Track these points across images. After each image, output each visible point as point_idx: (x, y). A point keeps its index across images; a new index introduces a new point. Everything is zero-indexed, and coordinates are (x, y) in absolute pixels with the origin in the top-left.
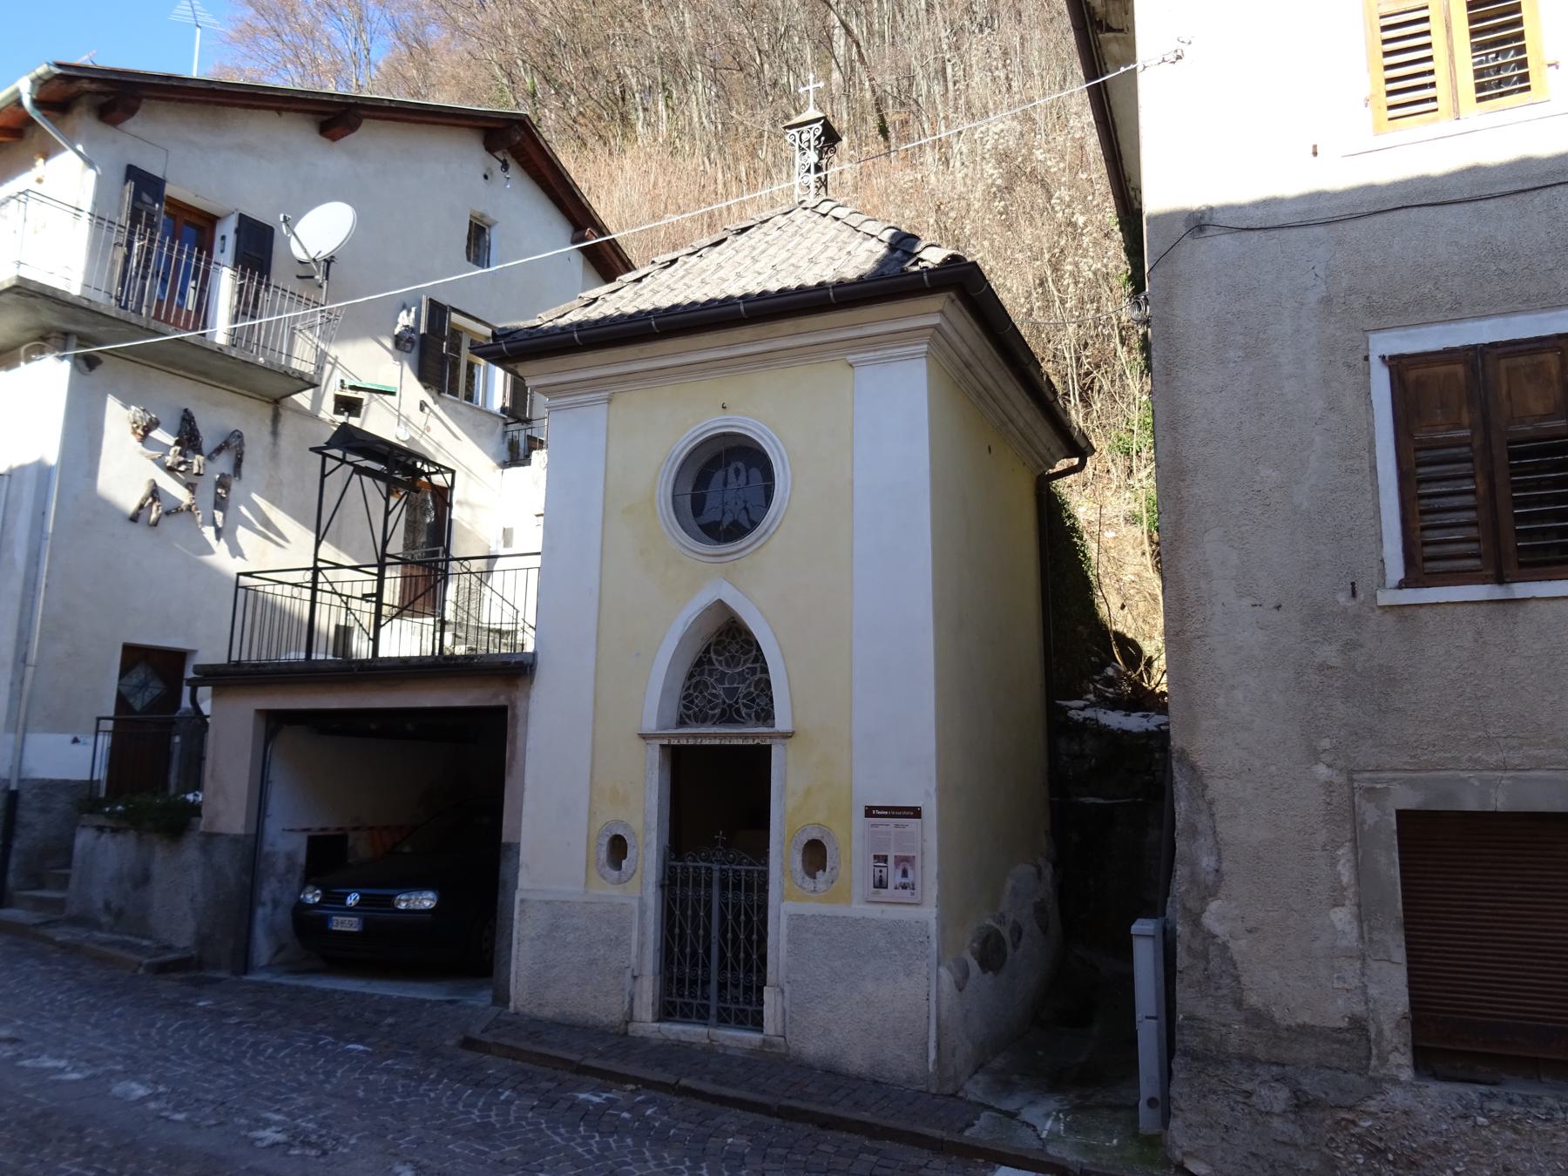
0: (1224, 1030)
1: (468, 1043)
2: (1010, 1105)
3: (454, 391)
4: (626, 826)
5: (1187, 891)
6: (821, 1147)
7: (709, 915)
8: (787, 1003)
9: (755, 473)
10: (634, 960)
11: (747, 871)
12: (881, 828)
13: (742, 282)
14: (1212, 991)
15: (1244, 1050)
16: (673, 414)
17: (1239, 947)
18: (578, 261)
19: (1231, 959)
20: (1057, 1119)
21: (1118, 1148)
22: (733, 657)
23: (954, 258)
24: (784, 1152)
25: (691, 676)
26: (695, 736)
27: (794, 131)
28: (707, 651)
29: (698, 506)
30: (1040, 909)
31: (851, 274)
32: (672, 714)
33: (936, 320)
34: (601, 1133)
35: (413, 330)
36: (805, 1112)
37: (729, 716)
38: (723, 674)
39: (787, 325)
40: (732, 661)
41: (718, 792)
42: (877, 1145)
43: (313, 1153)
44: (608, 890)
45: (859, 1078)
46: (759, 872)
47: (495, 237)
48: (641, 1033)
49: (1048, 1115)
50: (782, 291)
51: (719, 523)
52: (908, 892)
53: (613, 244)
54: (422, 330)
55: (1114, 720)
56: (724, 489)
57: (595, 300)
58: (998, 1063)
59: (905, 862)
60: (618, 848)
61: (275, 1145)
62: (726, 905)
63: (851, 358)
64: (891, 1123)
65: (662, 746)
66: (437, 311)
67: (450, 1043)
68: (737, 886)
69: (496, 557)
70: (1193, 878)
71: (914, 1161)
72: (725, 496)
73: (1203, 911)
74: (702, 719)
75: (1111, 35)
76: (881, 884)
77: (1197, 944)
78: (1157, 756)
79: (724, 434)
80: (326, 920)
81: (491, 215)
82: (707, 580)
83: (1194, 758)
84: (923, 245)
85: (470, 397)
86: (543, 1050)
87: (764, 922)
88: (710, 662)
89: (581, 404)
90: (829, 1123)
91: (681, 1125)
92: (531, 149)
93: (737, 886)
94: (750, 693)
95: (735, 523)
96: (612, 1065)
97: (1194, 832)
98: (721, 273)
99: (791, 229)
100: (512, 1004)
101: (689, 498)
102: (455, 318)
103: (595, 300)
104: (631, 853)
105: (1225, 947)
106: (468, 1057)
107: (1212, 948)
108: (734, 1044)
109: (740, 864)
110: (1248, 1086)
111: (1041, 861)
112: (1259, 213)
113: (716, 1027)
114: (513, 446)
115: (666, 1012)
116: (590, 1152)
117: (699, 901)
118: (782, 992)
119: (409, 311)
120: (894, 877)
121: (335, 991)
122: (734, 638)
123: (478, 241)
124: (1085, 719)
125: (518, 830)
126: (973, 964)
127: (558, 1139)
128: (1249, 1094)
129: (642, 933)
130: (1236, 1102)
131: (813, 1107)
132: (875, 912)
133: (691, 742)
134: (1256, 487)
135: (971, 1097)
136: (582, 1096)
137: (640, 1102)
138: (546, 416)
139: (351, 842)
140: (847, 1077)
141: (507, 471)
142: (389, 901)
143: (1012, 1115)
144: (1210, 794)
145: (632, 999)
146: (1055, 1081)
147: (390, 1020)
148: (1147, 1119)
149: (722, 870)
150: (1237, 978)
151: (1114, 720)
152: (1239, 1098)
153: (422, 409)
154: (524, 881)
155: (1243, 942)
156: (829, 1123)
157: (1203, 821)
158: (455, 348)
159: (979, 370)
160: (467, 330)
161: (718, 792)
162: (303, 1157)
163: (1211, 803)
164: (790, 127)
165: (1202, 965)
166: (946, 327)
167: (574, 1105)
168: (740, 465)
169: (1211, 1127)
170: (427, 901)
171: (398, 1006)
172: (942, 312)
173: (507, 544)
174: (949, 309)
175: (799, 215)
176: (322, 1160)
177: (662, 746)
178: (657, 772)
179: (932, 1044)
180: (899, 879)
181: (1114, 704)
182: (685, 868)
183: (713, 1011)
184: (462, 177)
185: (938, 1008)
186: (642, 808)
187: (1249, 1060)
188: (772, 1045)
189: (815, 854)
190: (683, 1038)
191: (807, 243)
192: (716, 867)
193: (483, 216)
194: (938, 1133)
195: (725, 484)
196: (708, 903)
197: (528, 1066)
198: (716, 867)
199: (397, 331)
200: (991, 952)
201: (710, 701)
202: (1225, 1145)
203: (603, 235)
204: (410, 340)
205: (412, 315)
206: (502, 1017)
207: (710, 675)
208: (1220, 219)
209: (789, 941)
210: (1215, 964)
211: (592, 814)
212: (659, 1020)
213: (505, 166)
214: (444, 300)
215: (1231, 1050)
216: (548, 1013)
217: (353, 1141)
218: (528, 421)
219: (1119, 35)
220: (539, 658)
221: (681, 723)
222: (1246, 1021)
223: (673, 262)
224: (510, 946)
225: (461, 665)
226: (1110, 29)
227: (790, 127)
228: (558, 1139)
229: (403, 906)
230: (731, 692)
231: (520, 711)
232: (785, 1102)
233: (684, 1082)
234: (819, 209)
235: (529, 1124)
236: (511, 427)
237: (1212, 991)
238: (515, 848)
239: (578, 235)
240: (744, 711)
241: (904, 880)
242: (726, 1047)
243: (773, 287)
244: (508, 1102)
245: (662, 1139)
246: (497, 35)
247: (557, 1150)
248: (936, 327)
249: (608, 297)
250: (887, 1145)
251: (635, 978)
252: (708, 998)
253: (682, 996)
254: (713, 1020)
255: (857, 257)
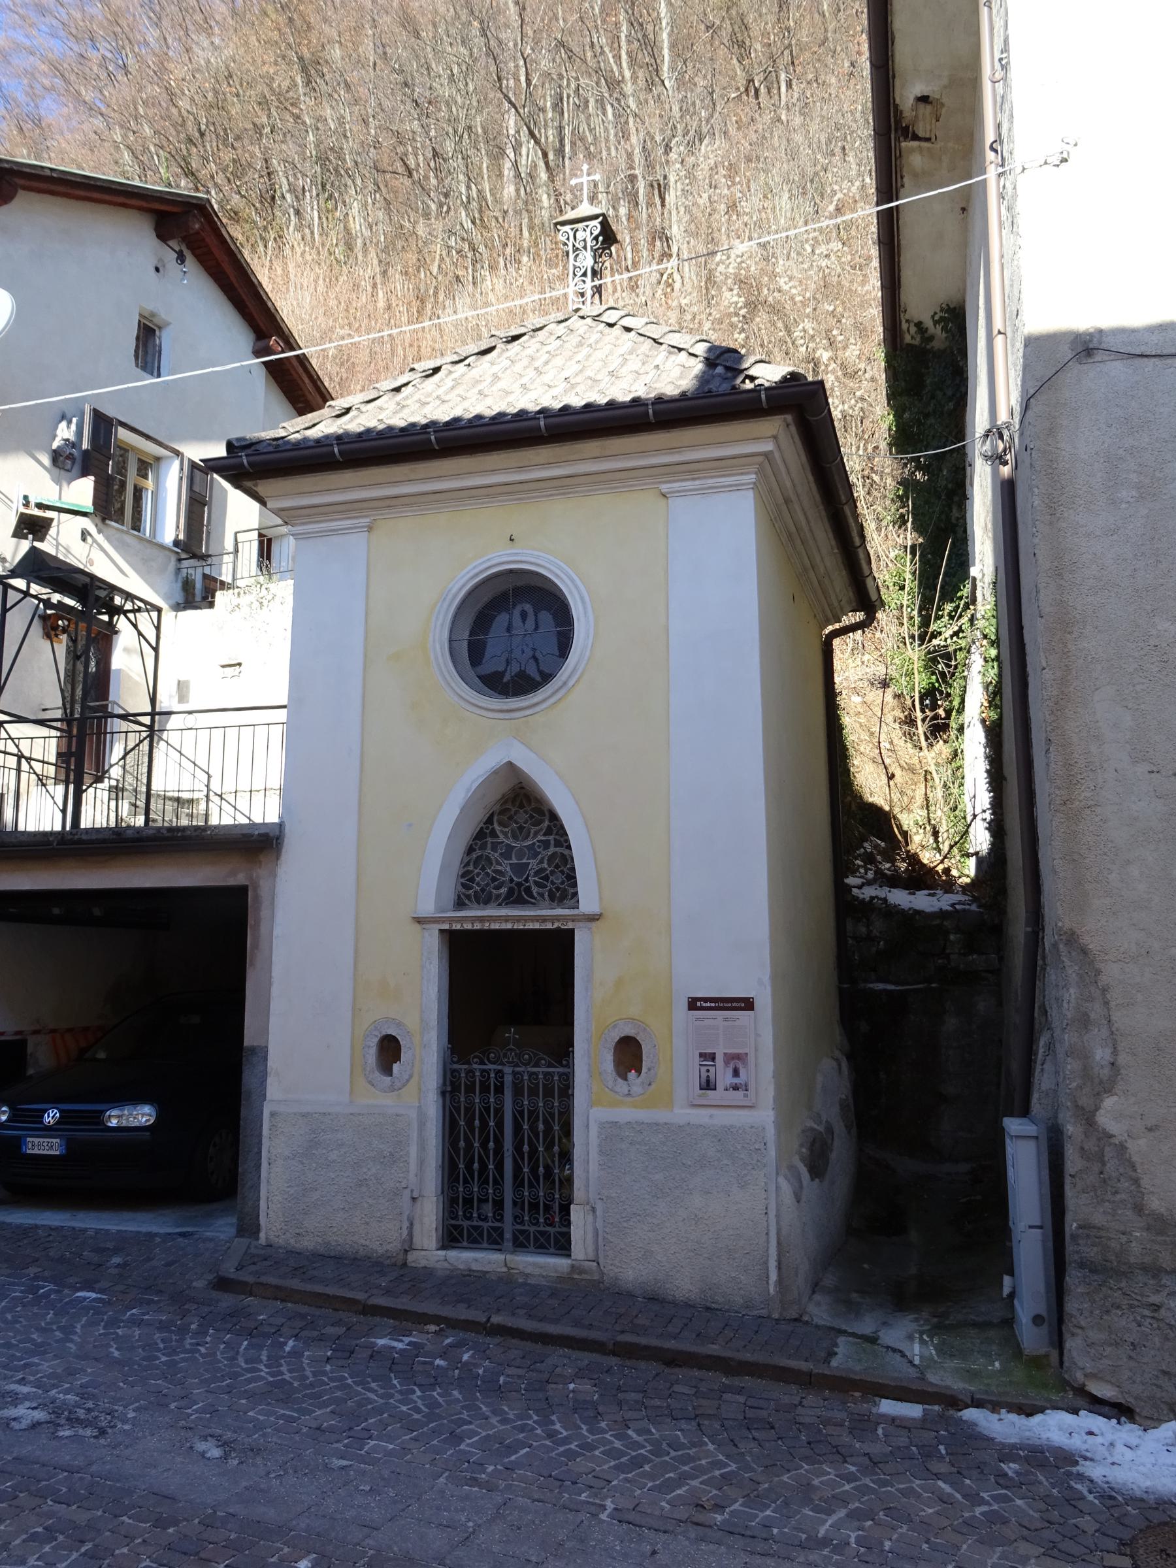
0: (1124, 1239)
1: (223, 1284)
2: (866, 1327)
3: (120, 519)
4: (399, 1024)
5: (1080, 1087)
6: (676, 1388)
7: (500, 1125)
8: (599, 1224)
9: (546, 617)
10: (412, 1176)
11: (546, 1074)
12: (707, 1022)
13: (532, 395)
14: (1109, 1196)
15: (1147, 1260)
16: (455, 543)
17: (1138, 1147)
18: (260, 381)
19: (1129, 1161)
20: (923, 1342)
21: (1002, 1371)
22: (521, 828)
23: (794, 377)
24: (639, 1396)
25: (470, 850)
26: (482, 919)
27: (567, 228)
28: (490, 821)
29: (476, 652)
30: (843, 1106)
31: (671, 391)
32: (450, 896)
33: (768, 446)
34: (420, 1386)
35: (73, 445)
36: (647, 1347)
37: (517, 896)
38: (510, 848)
39: (592, 447)
40: (520, 833)
41: (509, 986)
42: (737, 1382)
43: (88, 1432)
44: (378, 1098)
45: (688, 1305)
46: (561, 1075)
47: (167, 340)
48: (423, 1263)
49: (910, 1338)
50: (588, 407)
51: (502, 674)
52: (740, 1093)
53: (303, 360)
54: (85, 446)
55: (899, 898)
56: (512, 634)
57: (348, 410)
58: (829, 1280)
59: (736, 1061)
60: (389, 1050)
61: (35, 1425)
62: (521, 1113)
63: (665, 488)
64: (748, 1356)
65: (441, 931)
66: (103, 424)
67: (199, 1284)
68: (533, 1092)
69: (170, 713)
70: (1086, 1073)
71: (786, 1399)
72: (512, 638)
73: (1097, 1108)
74: (484, 899)
75: (915, 144)
76: (708, 1085)
77: (1091, 1145)
78: (952, 937)
79: (511, 571)
80: (18, 1142)
81: (163, 315)
82: (486, 741)
83: (1086, 940)
84: (752, 359)
85: (137, 525)
86: (319, 1289)
87: (567, 1130)
88: (493, 834)
89: (335, 532)
90: (673, 1360)
91: (509, 1371)
92: (211, 241)
93: (533, 1092)
94: (542, 870)
95: (522, 675)
96: (403, 1303)
97: (1084, 1022)
98: (501, 385)
99: (574, 340)
100: (262, 1235)
101: (465, 644)
102: (122, 433)
103: (348, 410)
104: (404, 1056)
105: (1122, 1148)
106: (227, 1301)
107: (1107, 1149)
108: (537, 1271)
109: (537, 1065)
110: (1155, 1299)
111: (837, 1054)
112: (1154, 338)
113: (513, 1253)
114: (187, 586)
115: (451, 1238)
116: (417, 1410)
117: (488, 1110)
118: (594, 1210)
119: (70, 422)
120: (724, 1077)
121: (36, 1227)
122: (521, 806)
123: (147, 343)
124: (872, 898)
125: (265, 1030)
126: (804, 1170)
127: (372, 1396)
128: (1156, 1307)
129: (422, 1147)
130: (1144, 1317)
131: (654, 1342)
132: (701, 1116)
133: (477, 926)
134: (1152, 642)
135: (816, 1321)
136: (381, 1342)
137: (450, 1346)
138: (285, 549)
139: (30, 1049)
140: (674, 1303)
141: (180, 614)
142: (97, 1119)
143: (873, 1340)
144: (1104, 980)
145: (412, 1224)
146: (902, 1299)
147: (116, 1260)
148: (1031, 1338)
149: (514, 1073)
150: (1136, 1182)
151: (899, 898)
152: (1147, 1313)
153: (84, 540)
154: (273, 1090)
155: (1142, 1142)
156: (673, 1360)
157: (1096, 1011)
158: (122, 468)
159: (797, 507)
160: (134, 449)
161: (509, 986)
162: (76, 1438)
163: (1104, 990)
164: (563, 223)
165: (1096, 1168)
166: (777, 455)
167: (375, 1355)
168: (528, 607)
169: (1117, 1344)
170: (143, 1115)
171: (122, 1242)
172: (775, 437)
173: (182, 698)
174: (782, 437)
175: (574, 322)
176: (102, 1441)
177: (441, 931)
178: (435, 962)
179: (773, 1264)
180: (729, 1079)
181: (894, 881)
182: (470, 1072)
183: (508, 1235)
184: (129, 269)
185: (778, 1223)
186: (418, 1003)
187: (1154, 1271)
188: (582, 1271)
189: (629, 1054)
190: (475, 1267)
191: (599, 354)
192: (508, 1070)
193: (153, 315)
194: (804, 1366)
195: (509, 629)
196: (499, 1112)
197: (304, 1309)
198: (508, 1070)
199: (55, 445)
200: (817, 1159)
201: (494, 879)
202: (1132, 1364)
203: (293, 349)
204: (70, 457)
205: (73, 427)
206: (253, 1250)
207: (494, 849)
208: (1110, 343)
209: (601, 1152)
210: (1111, 1167)
211: (356, 1011)
212: (443, 1247)
213: (181, 258)
214: (110, 411)
215: (1132, 1260)
216: (307, 1244)
217: (131, 1415)
218: (204, 557)
219: (925, 144)
220: (287, 829)
221: (460, 904)
222: (1148, 1229)
223: (436, 370)
224: (258, 1166)
225: (190, 838)
226: (916, 137)
227: (563, 223)
228: (372, 1396)
229: (114, 1122)
230: (520, 869)
231: (264, 891)
232: (621, 1338)
233: (496, 1319)
234: (605, 318)
235: (332, 1379)
236: (185, 563)
237: (1109, 1196)
238: (261, 1053)
239: (261, 344)
240: (535, 890)
241: (736, 1080)
242: (527, 1275)
243: (577, 402)
244: (296, 1354)
245: (492, 1389)
246: (129, 118)
247: (378, 1411)
248: (767, 455)
249: (364, 408)
250: (747, 1381)
251: (414, 1199)
252: (501, 1220)
253: (537, 1224)
254: (508, 1244)
255: (676, 375)
